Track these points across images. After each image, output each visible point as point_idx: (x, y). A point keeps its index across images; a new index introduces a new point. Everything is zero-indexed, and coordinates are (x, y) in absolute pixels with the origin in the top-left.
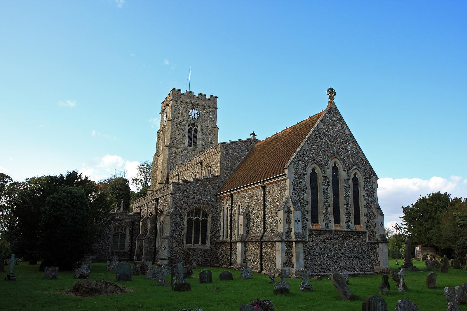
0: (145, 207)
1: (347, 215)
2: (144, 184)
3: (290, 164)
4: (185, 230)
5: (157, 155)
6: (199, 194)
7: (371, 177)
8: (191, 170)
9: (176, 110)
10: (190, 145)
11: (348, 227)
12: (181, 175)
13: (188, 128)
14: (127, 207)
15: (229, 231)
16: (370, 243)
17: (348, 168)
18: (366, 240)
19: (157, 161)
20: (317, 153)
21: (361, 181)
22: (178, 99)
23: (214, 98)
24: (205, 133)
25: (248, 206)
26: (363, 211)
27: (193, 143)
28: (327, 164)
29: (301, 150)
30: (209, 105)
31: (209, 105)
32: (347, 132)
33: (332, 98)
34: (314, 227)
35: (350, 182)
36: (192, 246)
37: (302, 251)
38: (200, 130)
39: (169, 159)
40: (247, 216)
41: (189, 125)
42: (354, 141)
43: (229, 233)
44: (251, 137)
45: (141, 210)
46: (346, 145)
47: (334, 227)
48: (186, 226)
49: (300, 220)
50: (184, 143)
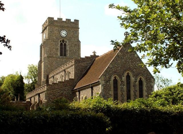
0: (33, 98)
2: (33, 79)
3: (102, 76)
5: (41, 62)
6: (62, 90)
9: (51, 32)
10: (61, 55)
12: (55, 77)
13: (60, 43)
14: (23, 98)
17: (136, 76)
21: (144, 82)
22: (53, 25)
23: (77, 22)
24: (72, 46)
25: (86, 97)
27: (63, 54)
28: (123, 74)
29: (108, 68)
30: (73, 26)
35: (137, 83)
41: (60, 41)
44: (93, 54)
45: (31, 100)
46: (135, 63)
50: (58, 54)
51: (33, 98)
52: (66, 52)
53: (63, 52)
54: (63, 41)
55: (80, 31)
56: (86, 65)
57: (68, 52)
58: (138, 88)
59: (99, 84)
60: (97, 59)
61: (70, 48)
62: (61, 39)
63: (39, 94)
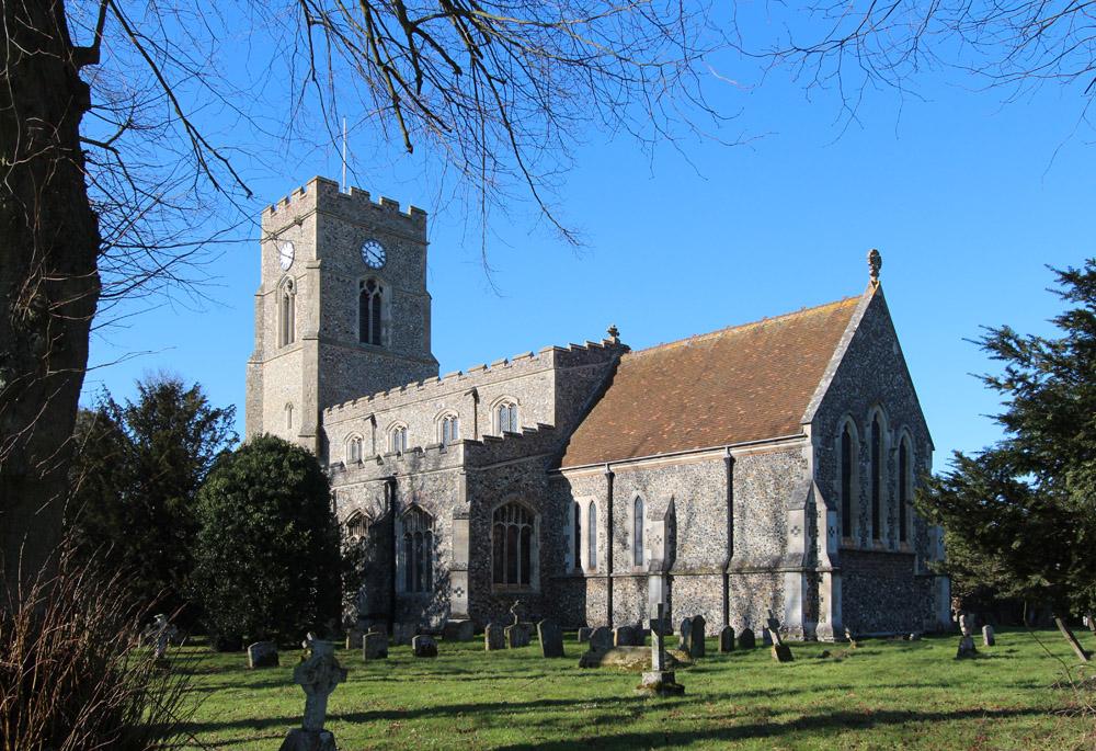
1: (891, 520)
10: (364, 338)
11: (892, 544)
13: (359, 291)
17: (895, 426)
19: (261, 375)
32: (895, 348)
38: (388, 301)
41: (361, 286)
47: (872, 545)
56: (591, 377)
60: (624, 358)
62: (365, 277)
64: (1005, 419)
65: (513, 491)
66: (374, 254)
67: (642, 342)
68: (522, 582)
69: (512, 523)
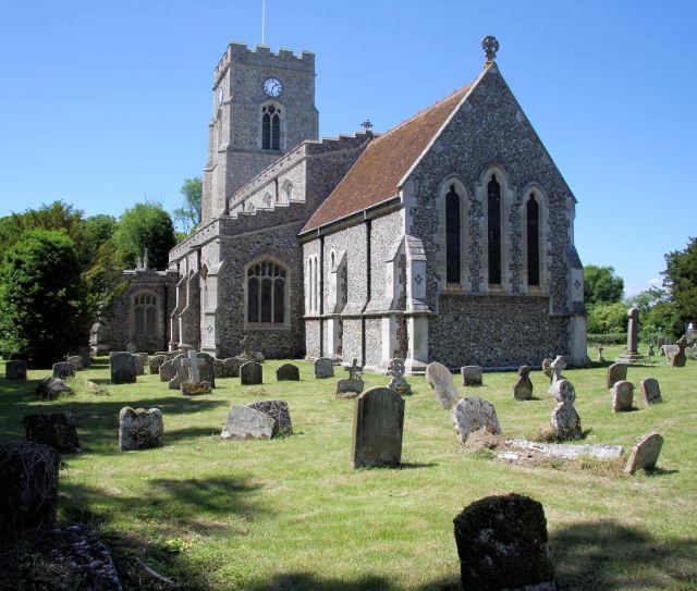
1: (515, 267)
4: (246, 299)
7: (562, 198)
8: (262, 193)
10: (266, 146)
13: (262, 115)
15: (319, 299)
16: (557, 317)
17: (520, 184)
18: (547, 311)
20: (459, 159)
23: (309, 59)
24: (294, 124)
25: (346, 254)
26: (545, 260)
28: (478, 178)
30: (299, 71)
31: (299, 71)
33: (490, 55)
34: (451, 289)
35: (523, 209)
36: (259, 326)
37: (425, 329)
39: (228, 173)
40: (343, 272)
41: (264, 110)
42: (532, 133)
43: (319, 303)
47: (488, 290)
48: (246, 293)
49: (424, 277)
51: (185, 260)
52: (278, 138)
53: (271, 126)
54: (272, 109)
55: (317, 80)
57: (286, 139)
58: (523, 228)
59: (398, 209)
61: (289, 128)
63: (198, 249)
64: (71, 207)
65: (264, 252)
66: (272, 87)
67: (382, 129)
68: (275, 321)
69: (267, 277)
